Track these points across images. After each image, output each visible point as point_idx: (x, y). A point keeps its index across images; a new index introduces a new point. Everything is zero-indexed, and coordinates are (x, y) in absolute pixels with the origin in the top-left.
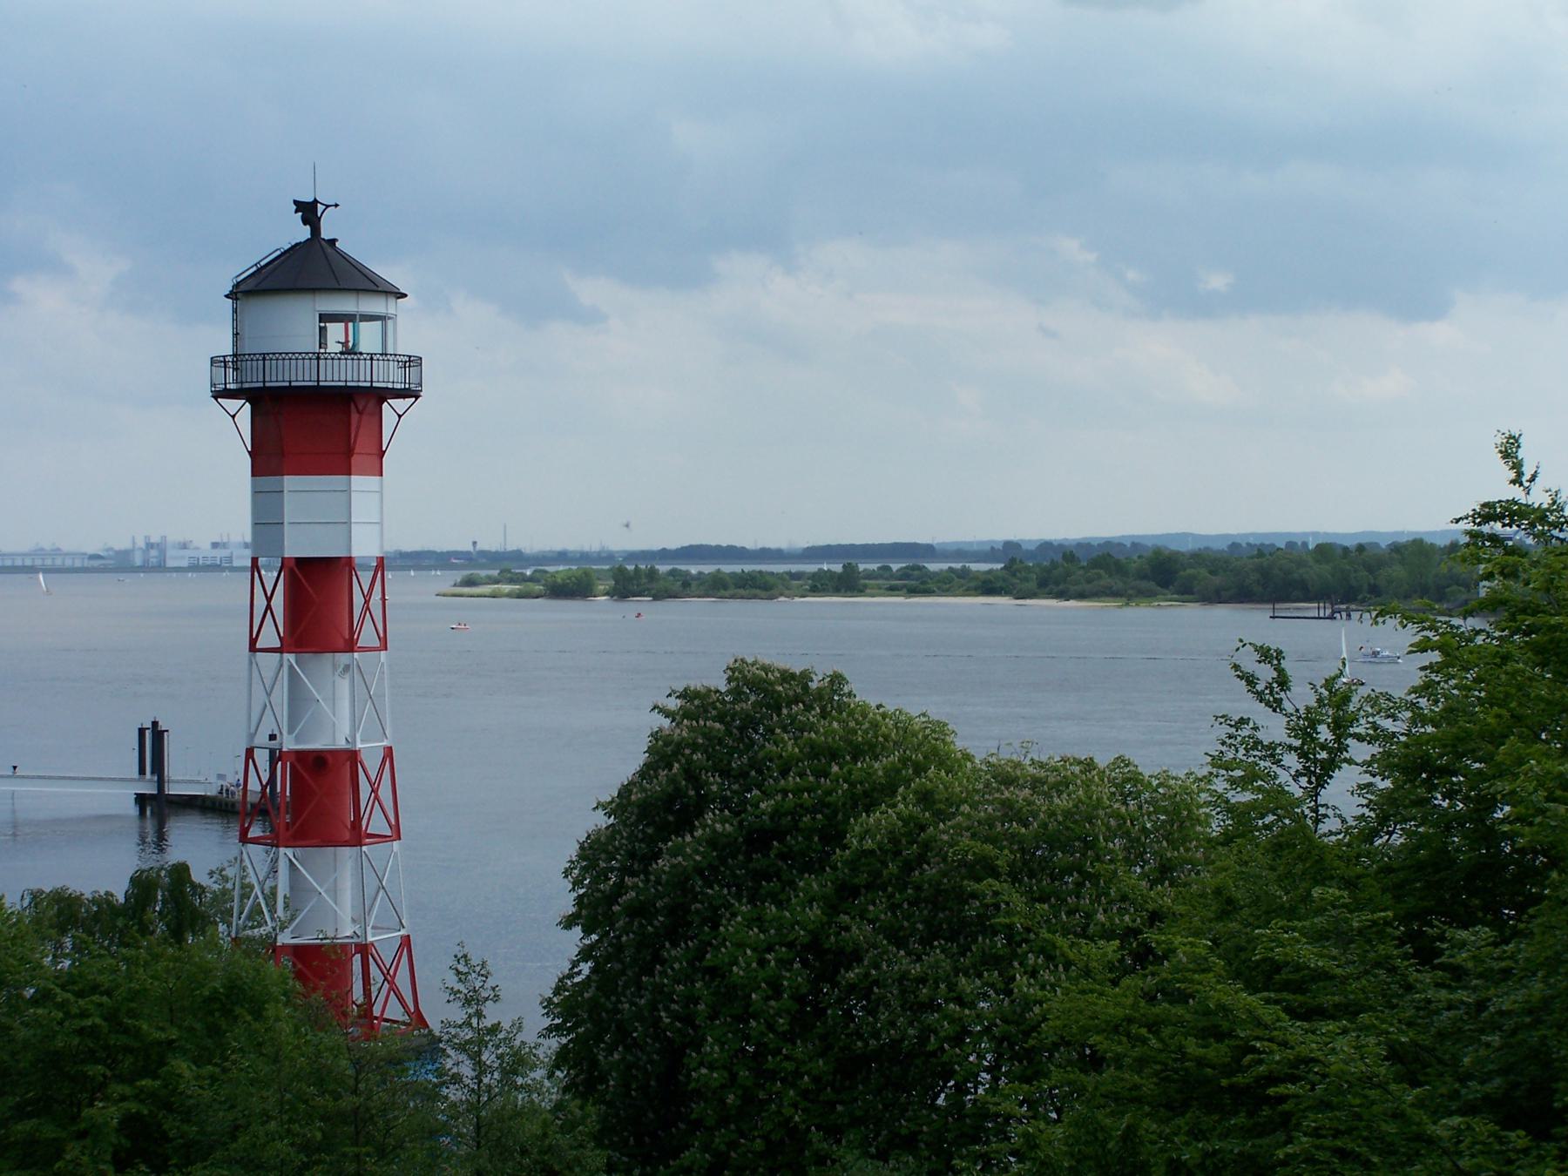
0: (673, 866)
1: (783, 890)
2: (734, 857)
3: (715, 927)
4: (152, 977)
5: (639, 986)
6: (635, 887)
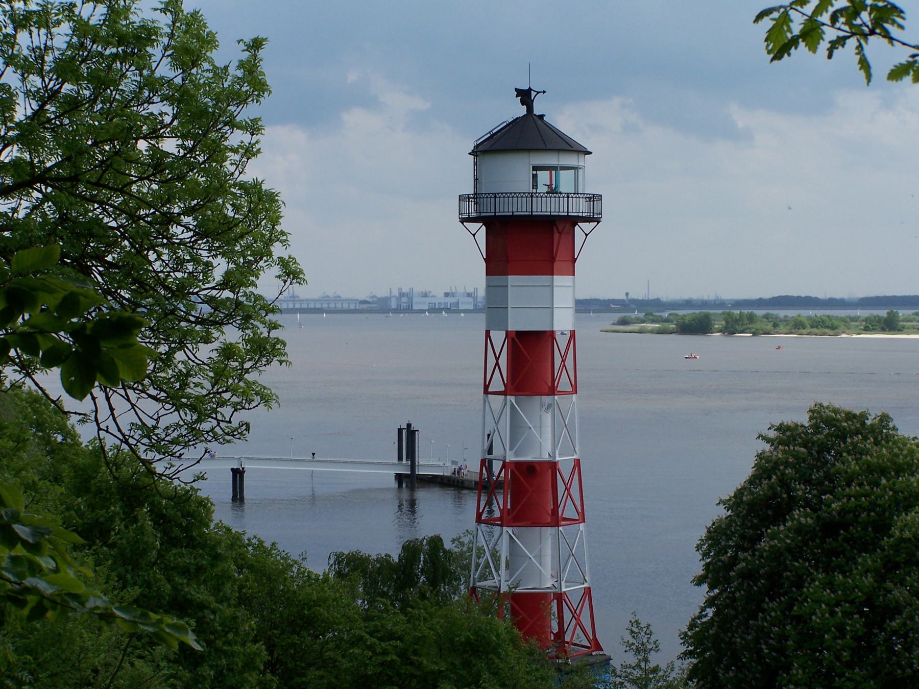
0: (771, 546)
1: (847, 563)
2: (813, 540)
3: (799, 586)
4: (429, 629)
5: (748, 627)
6: (745, 559)
